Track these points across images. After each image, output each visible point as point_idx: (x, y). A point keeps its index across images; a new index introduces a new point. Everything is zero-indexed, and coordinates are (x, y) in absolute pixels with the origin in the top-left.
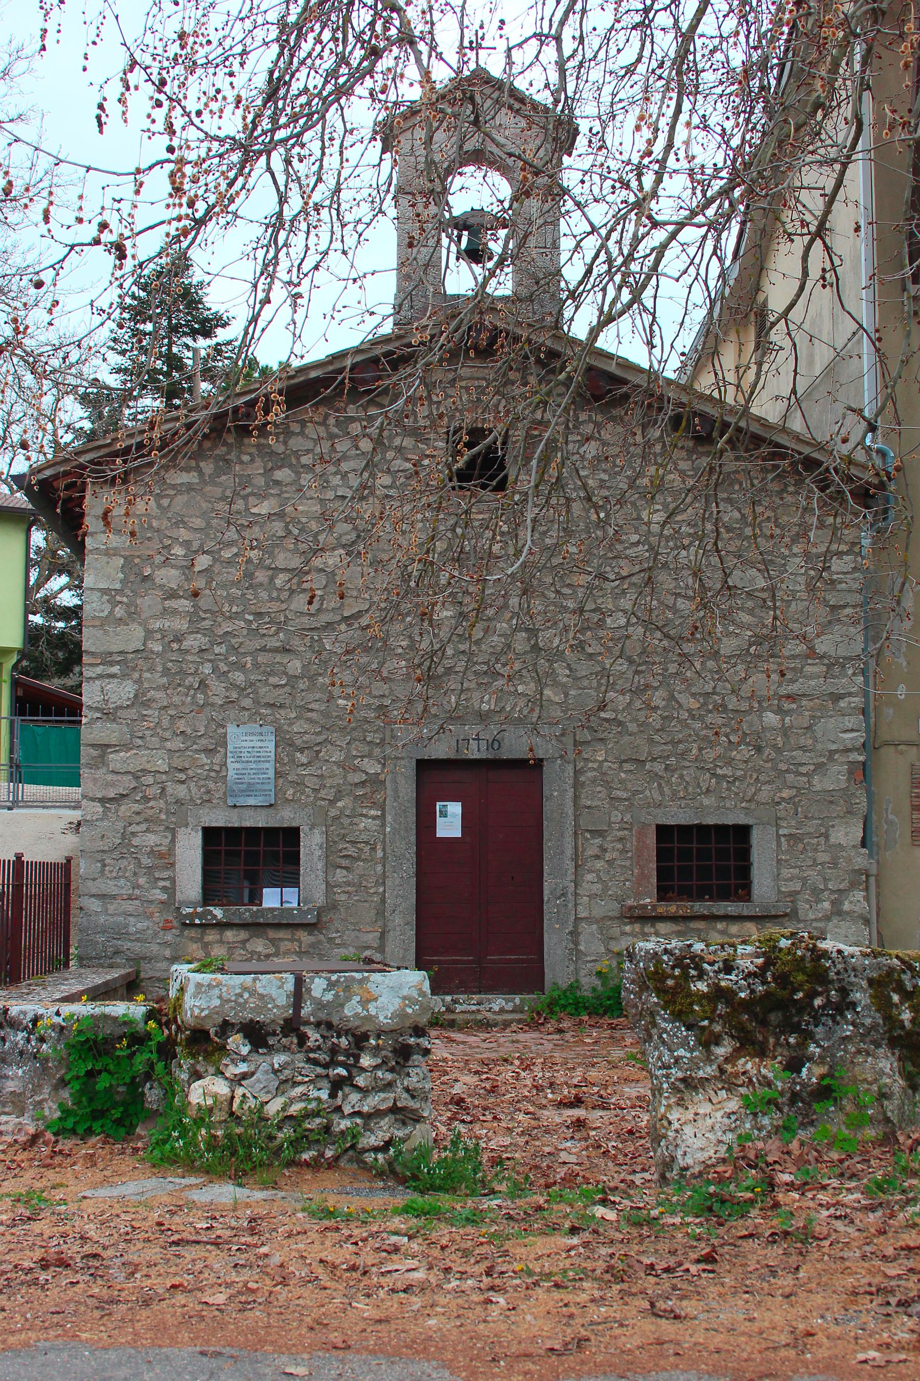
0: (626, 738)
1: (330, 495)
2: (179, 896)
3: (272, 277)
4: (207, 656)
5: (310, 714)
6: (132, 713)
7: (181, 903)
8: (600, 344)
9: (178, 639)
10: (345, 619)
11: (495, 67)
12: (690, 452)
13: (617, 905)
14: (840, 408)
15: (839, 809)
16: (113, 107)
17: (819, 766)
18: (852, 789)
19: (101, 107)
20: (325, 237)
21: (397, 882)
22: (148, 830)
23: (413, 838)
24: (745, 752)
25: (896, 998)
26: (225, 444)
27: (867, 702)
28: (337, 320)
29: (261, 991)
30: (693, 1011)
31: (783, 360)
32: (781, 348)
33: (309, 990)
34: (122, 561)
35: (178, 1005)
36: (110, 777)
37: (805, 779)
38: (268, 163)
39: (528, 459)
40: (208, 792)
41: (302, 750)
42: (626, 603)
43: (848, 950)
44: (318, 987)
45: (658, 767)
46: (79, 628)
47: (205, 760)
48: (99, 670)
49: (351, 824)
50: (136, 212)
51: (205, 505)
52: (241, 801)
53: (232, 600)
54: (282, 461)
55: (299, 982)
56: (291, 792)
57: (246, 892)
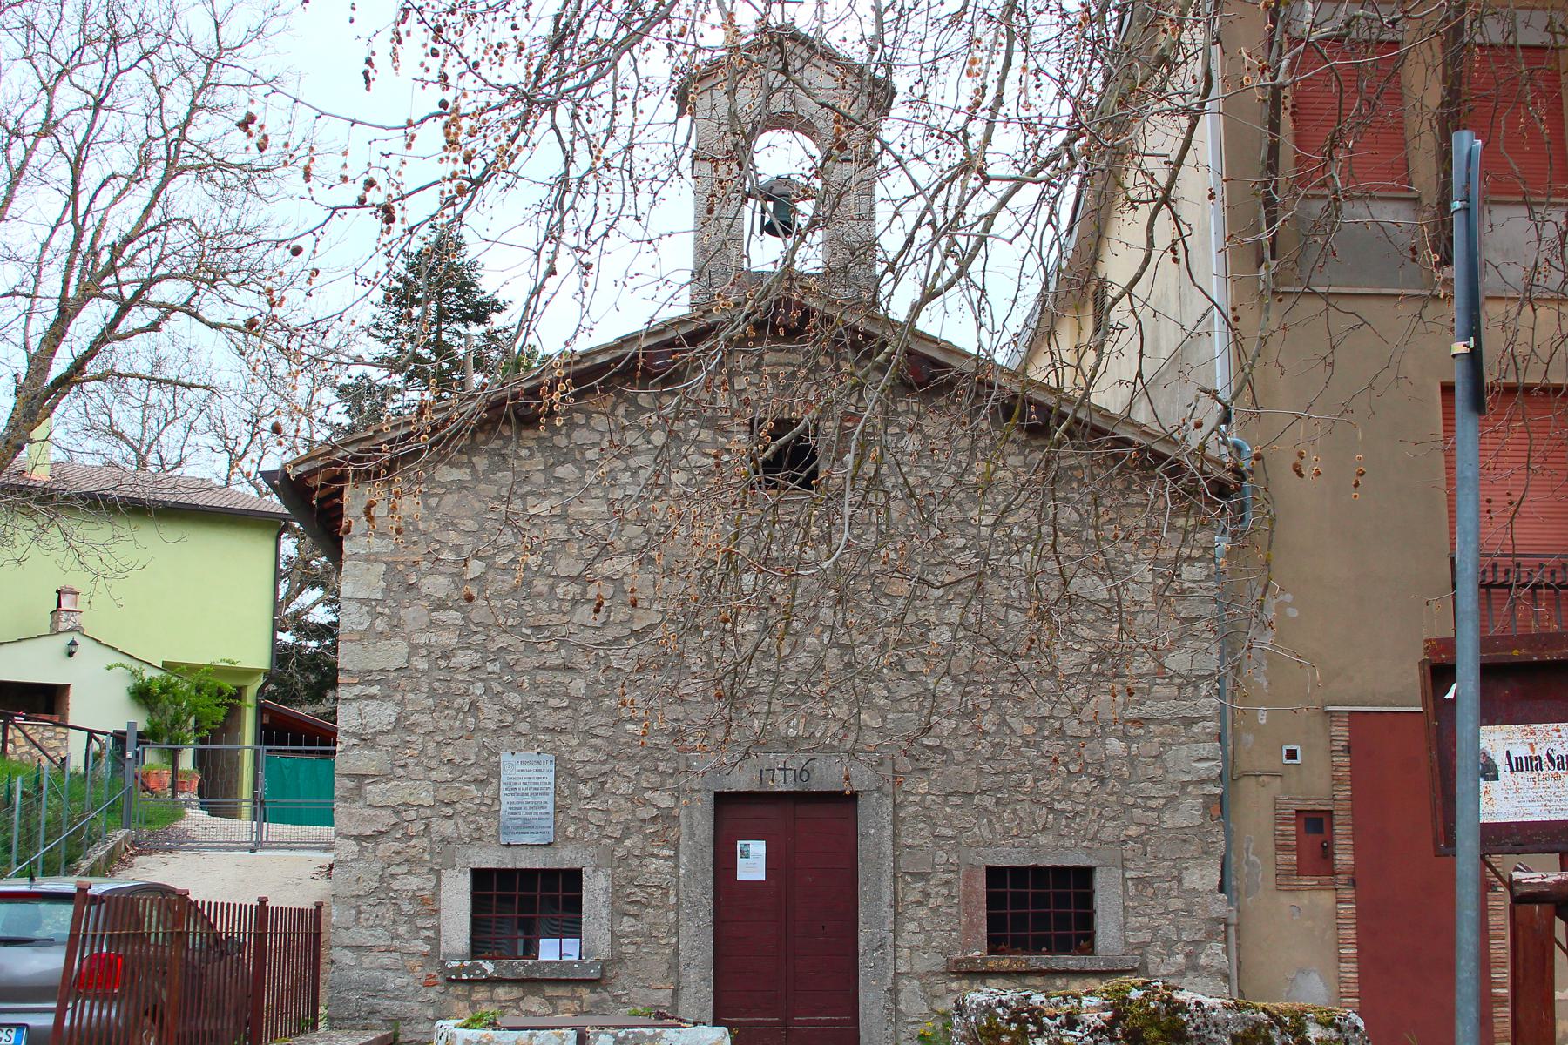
0: (952, 768)
1: (618, 494)
2: (444, 948)
3: (558, 240)
4: (478, 674)
5: (594, 741)
6: (393, 739)
7: (446, 955)
9: (446, 655)
10: (635, 633)
13: (941, 959)
14: (1190, 392)
15: (1192, 849)
16: (382, 61)
17: (1170, 800)
18: (1209, 824)
19: (369, 62)
20: (616, 201)
21: (692, 931)
22: (409, 872)
23: (711, 882)
24: (1086, 784)
26: (501, 436)
27: (1223, 728)
28: (629, 288)
31: (1126, 342)
34: (384, 567)
36: (367, 812)
37: (1155, 815)
38: (553, 120)
39: (841, 455)
40: (479, 829)
42: (953, 615)
43: (1208, 1002)
45: (988, 801)
47: (475, 793)
48: (357, 690)
51: (477, 505)
52: (515, 839)
53: (507, 612)
54: (565, 456)
56: (572, 828)
57: (521, 943)
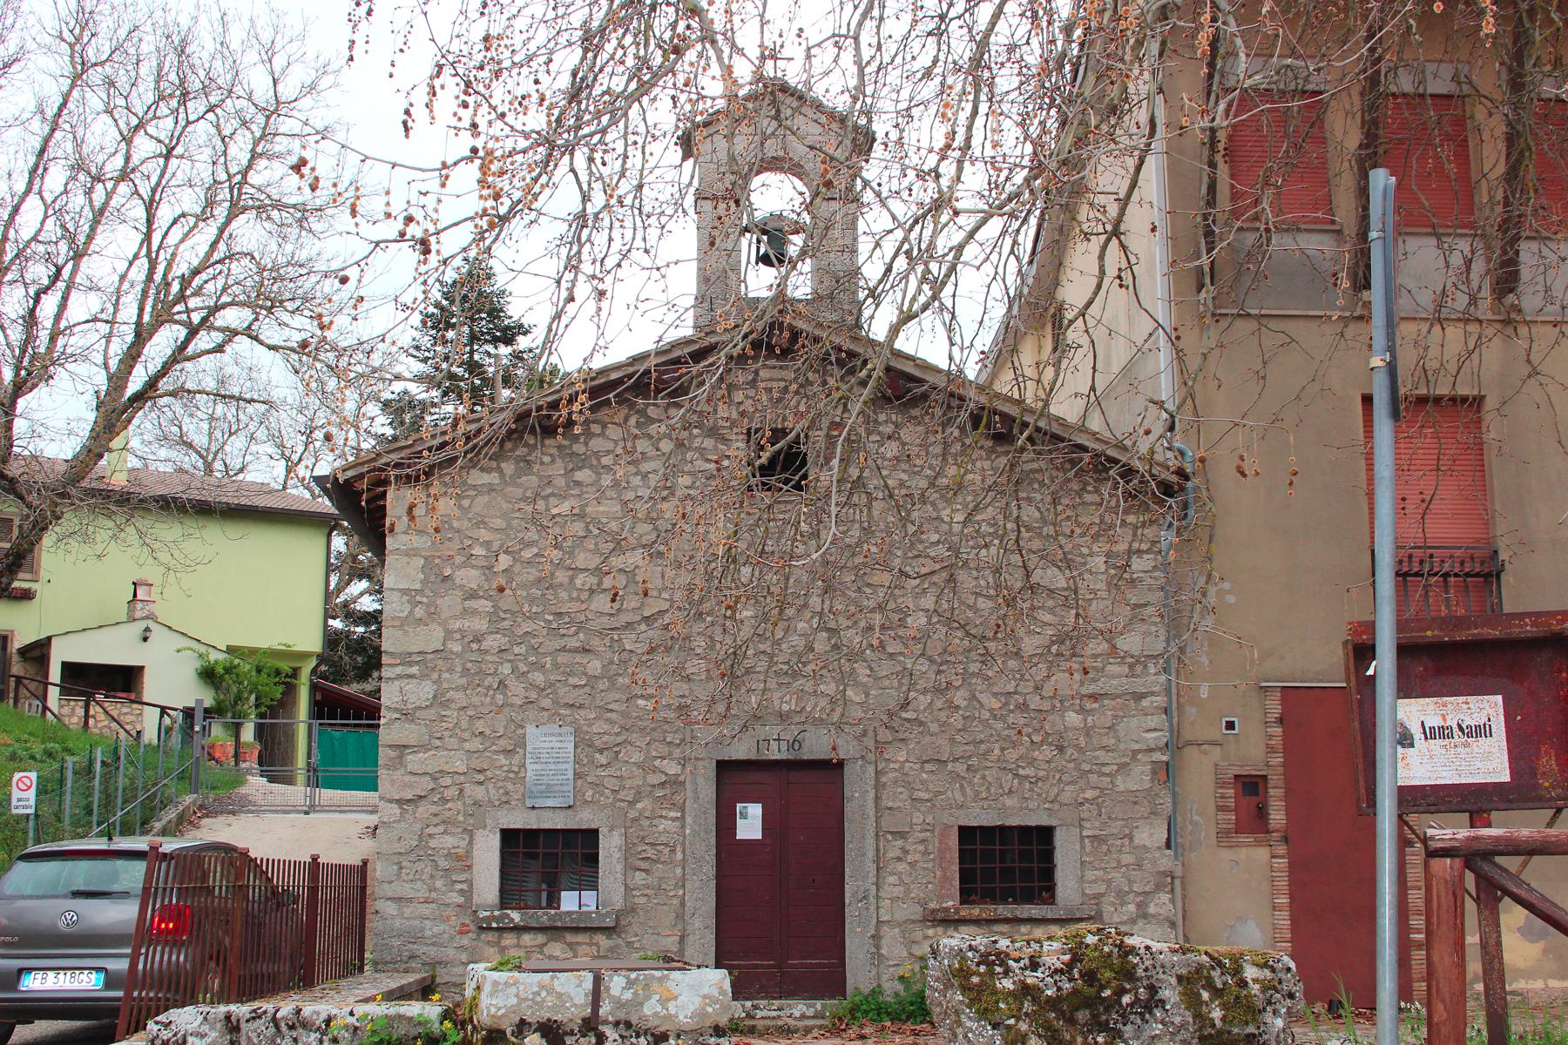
0: (928, 739)
2: (476, 900)
6: (431, 714)
8: (898, 345)
9: (478, 639)
11: (793, 74)
12: (991, 451)
14: (1140, 403)
15: (1143, 810)
16: (420, 112)
18: (1156, 788)
19: (407, 112)
20: (629, 234)
22: (445, 832)
23: (713, 841)
24: (1047, 752)
25: (1205, 995)
26: (527, 445)
29: (558, 989)
30: (998, 1009)
31: (1081, 359)
32: (1080, 346)
33: (608, 989)
34: (422, 561)
35: (474, 1005)
36: (408, 778)
39: (828, 460)
41: (601, 751)
43: (1155, 946)
44: (616, 984)
45: (960, 768)
46: (379, 634)
48: (399, 670)
49: (651, 825)
50: (440, 207)
51: (505, 506)
52: (539, 803)
54: (582, 462)
55: (598, 980)
56: (590, 793)
57: (544, 895)
